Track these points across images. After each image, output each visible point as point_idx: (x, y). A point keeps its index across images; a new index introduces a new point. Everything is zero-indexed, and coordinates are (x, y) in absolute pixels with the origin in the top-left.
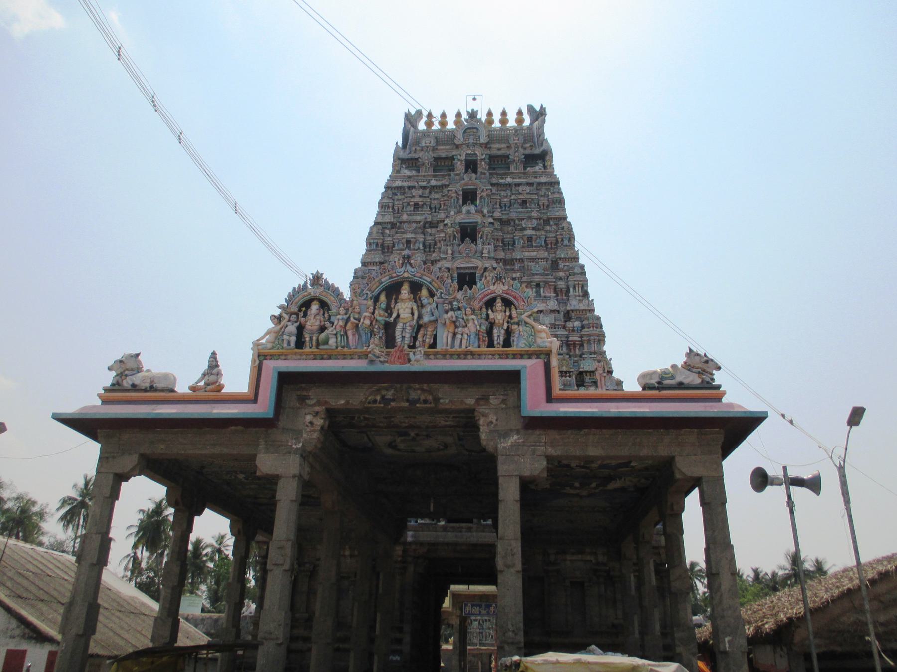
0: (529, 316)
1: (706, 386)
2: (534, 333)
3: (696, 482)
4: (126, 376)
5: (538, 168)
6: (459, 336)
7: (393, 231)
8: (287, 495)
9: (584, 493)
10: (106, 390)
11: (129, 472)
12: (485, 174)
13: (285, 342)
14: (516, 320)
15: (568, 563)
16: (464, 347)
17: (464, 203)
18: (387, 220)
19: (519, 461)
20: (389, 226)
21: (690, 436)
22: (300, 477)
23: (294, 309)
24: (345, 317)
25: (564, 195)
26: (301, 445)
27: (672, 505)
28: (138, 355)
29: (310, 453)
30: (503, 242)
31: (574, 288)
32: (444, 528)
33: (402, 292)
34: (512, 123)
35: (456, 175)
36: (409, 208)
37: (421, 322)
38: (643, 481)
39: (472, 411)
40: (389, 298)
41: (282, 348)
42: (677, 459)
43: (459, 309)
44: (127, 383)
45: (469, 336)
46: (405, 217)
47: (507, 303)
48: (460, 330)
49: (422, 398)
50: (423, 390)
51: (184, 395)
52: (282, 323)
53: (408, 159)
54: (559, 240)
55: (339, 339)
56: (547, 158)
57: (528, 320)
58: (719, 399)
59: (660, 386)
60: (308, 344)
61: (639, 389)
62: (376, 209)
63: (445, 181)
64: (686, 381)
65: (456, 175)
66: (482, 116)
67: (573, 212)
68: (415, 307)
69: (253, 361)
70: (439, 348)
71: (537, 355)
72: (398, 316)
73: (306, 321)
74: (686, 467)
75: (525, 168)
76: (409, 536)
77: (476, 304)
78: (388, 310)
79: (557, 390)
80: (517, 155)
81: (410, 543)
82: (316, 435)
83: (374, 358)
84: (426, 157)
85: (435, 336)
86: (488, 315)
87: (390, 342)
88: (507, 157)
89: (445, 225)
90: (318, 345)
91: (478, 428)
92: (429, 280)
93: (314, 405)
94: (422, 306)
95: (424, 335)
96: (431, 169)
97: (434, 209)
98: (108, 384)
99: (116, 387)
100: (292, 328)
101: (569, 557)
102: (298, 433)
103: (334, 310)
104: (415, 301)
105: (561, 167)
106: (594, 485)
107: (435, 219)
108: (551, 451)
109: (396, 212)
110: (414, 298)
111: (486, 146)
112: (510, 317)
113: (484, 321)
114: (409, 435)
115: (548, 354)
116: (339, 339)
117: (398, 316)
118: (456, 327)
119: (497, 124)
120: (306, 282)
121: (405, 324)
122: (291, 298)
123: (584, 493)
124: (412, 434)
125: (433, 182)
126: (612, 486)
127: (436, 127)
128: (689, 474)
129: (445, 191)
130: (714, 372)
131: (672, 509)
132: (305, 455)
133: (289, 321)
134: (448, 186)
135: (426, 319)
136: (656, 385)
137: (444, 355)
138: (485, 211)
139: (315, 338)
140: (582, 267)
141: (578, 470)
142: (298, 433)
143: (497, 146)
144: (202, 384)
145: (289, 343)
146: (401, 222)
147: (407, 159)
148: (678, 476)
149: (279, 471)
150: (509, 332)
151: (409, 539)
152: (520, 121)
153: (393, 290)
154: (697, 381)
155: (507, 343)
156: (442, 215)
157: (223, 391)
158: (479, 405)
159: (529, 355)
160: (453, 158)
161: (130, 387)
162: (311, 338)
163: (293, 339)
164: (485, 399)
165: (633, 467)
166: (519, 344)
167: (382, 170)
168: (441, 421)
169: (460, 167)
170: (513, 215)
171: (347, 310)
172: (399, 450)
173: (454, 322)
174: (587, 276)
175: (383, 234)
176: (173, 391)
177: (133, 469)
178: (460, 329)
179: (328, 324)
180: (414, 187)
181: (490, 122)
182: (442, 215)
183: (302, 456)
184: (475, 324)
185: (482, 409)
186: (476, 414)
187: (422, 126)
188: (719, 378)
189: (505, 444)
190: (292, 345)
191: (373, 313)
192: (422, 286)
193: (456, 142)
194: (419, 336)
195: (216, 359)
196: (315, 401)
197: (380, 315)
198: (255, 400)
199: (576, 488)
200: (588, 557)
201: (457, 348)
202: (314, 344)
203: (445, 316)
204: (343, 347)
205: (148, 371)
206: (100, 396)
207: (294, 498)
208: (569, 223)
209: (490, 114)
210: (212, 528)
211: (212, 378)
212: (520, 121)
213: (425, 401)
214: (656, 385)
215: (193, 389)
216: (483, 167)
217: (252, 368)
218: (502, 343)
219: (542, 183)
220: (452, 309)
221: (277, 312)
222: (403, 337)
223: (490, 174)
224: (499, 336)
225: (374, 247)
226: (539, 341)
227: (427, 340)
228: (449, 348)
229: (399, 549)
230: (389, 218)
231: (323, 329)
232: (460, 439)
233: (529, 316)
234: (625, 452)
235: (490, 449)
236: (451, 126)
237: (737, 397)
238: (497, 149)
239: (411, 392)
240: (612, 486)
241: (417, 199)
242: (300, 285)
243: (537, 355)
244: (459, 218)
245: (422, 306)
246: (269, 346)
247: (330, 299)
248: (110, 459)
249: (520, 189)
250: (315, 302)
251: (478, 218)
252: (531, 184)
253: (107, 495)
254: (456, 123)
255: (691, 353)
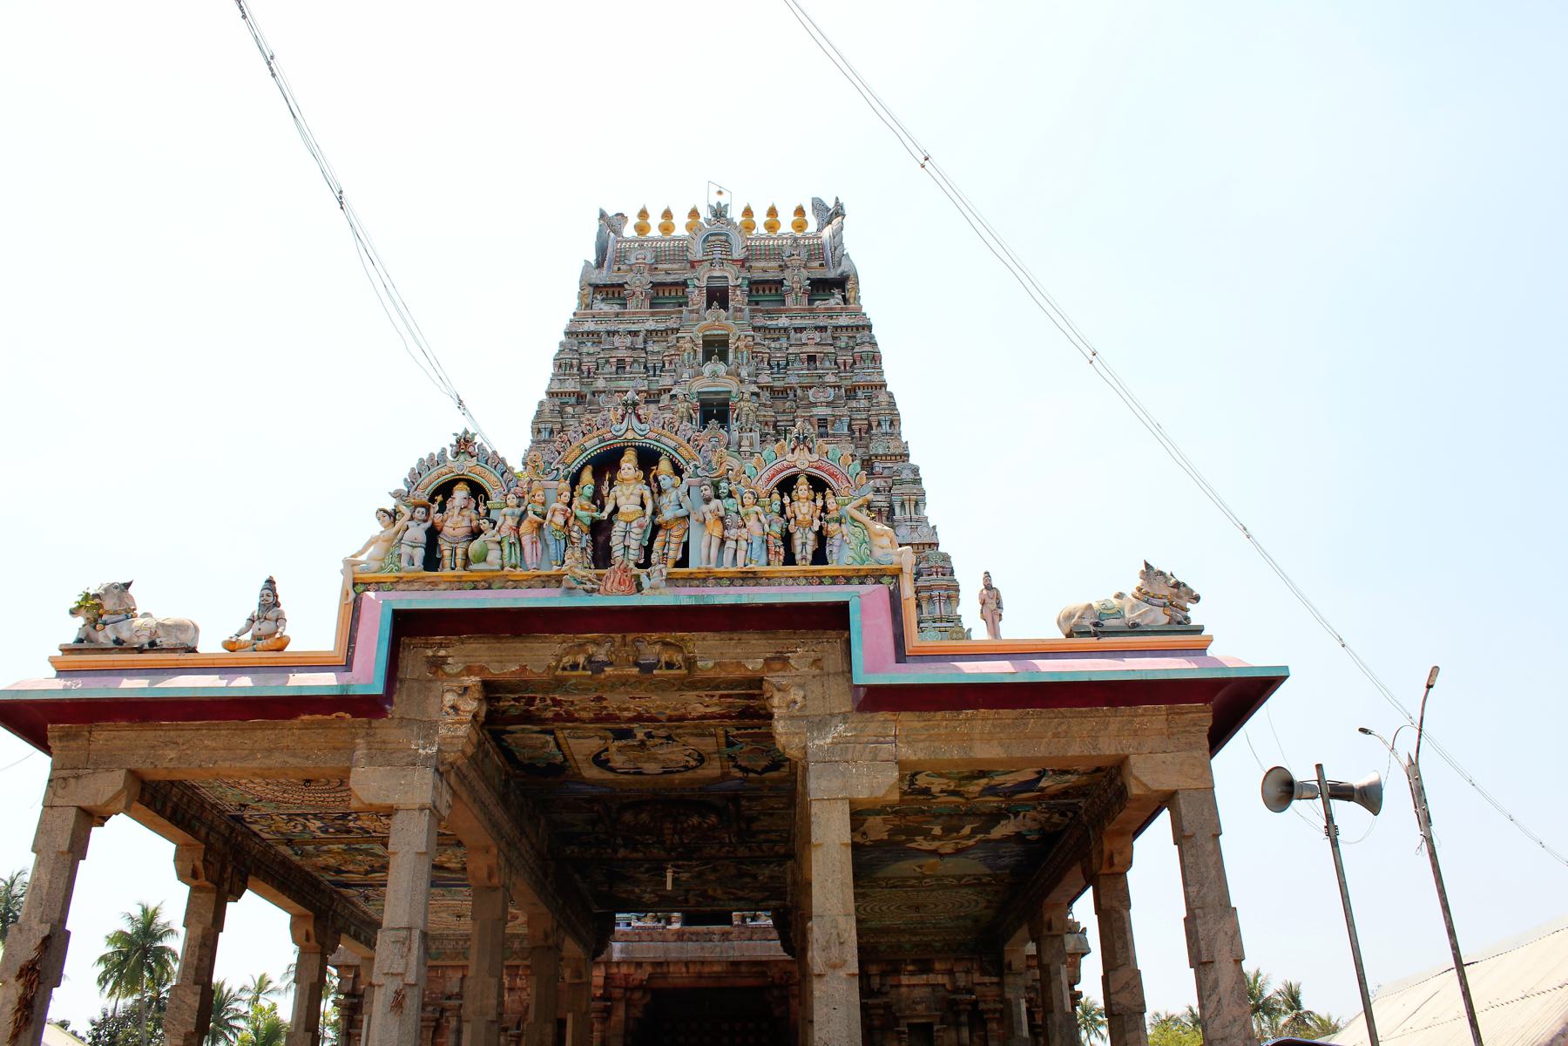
0: (859, 508)
1: (1178, 628)
2: (868, 540)
3: (1167, 800)
4: (105, 624)
5: (835, 301)
6: (730, 544)
7: (579, 409)
8: (409, 842)
9: (948, 847)
10: (67, 650)
11: (107, 804)
12: (741, 310)
13: (404, 560)
14: (834, 515)
15: (904, 990)
16: (740, 563)
17: (707, 358)
18: (571, 390)
19: (844, 773)
20: (573, 400)
21: (1154, 717)
22: (434, 810)
23: (424, 497)
24: (518, 511)
25: (881, 347)
26: (435, 749)
27: (1111, 856)
28: (127, 585)
29: (452, 764)
30: (775, 427)
31: (903, 505)
32: (680, 936)
33: (623, 465)
34: (786, 226)
35: (691, 312)
36: (608, 369)
37: (659, 520)
38: (1056, 818)
39: (757, 682)
40: (598, 476)
41: (399, 570)
42: (1132, 759)
43: (730, 495)
44: (105, 636)
45: (750, 544)
46: (600, 384)
47: (818, 485)
48: (732, 533)
49: (664, 658)
50: (665, 644)
51: (213, 657)
52: (398, 524)
53: (605, 286)
54: (874, 424)
55: (506, 551)
56: (849, 286)
57: (857, 514)
58: (1200, 650)
59: (1099, 630)
60: (447, 562)
61: (1059, 635)
62: (549, 369)
63: (672, 324)
64: (1143, 622)
65: (691, 312)
66: (736, 215)
67: (897, 374)
68: (647, 493)
69: (345, 594)
70: (695, 564)
71: (877, 576)
72: (616, 509)
73: (443, 521)
74: (1147, 774)
75: (811, 302)
76: (617, 950)
77: (762, 487)
78: (597, 499)
79: (914, 640)
80: (797, 279)
81: (618, 964)
82: (463, 730)
83: (574, 584)
84: (639, 283)
85: (686, 546)
86: (783, 506)
87: (602, 556)
88: (781, 282)
89: (673, 397)
90: (467, 561)
91: (770, 716)
92: (673, 444)
93: (459, 674)
94: (660, 492)
95: (665, 543)
96: (647, 303)
97: (651, 370)
98: (70, 638)
99: (85, 645)
100: (418, 533)
101: (905, 980)
102: (428, 728)
103: (495, 499)
104: (648, 484)
105: (872, 299)
106: (967, 830)
107: (654, 387)
108: (906, 752)
109: (588, 375)
110: (646, 477)
111: (743, 263)
112: (824, 509)
113: (775, 517)
114: (635, 736)
115: (896, 575)
116: (506, 551)
117: (616, 509)
118: (725, 527)
119: (760, 229)
120: (444, 450)
121: (629, 523)
122: (415, 477)
123: (948, 847)
124: (640, 735)
125: (651, 325)
126: (998, 832)
127: (655, 232)
128: (1155, 786)
129: (672, 338)
130: (1189, 605)
131: (1111, 864)
132: (443, 770)
133: (412, 519)
134: (678, 330)
135: (668, 514)
136: (1092, 628)
137: (704, 578)
138: (744, 373)
139: (460, 552)
140: (916, 470)
141: (944, 798)
142: (428, 728)
143: (763, 264)
144: (247, 637)
145: (411, 561)
146: (593, 394)
147: (602, 290)
148: (1135, 790)
149: (394, 799)
150: (821, 537)
151: (616, 956)
152: (800, 225)
153: (606, 464)
154: (1160, 618)
155: (820, 557)
156: (666, 381)
157: (287, 649)
158: (770, 670)
159: (862, 578)
160: (685, 284)
161: (112, 645)
162: (454, 551)
163: (420, 553)
164: (782, 660)
165: (1042, 789)
166: (842, 557)
167: (557, 305)
168: (696, 704)
169: (697, 298)
170: (793, 380)
171: (521, 498)
172: (612, 770)
173: (722, 519)
174: (925, 485)
175: (561, 412)
176: (194, 650)
177: (115, 798)
178: (733, 531)
179: (485, 524)
180: (614, 333)
181: (749, 226)
182: (666, 381)
183: (437, 770)
184: (759, 524)
185: (773, 678)
186: (766, 686)
187: (629, 232)
188: (1196, 615)
189: (821, 742)
190: (419, 561)
191: (570, 504)
192: (660, 454)
193: (690, 257)
194: (657, 545)
195: (274, 590)
196: (461, 667)
197: (583, 509)
198: (348, 666)
199: (935, 838)
200: (941, 979)
201: (727, 567)
202: (459, 561)
203: (705, 508)
204: (515, 567)
205: (146, 615)
206: (53, 661)
207: (423, 849)
208: (891, 395)
209: (748, 212)
210: (258, 943)
211: (266, 627)
212: (800, 225)
213: (670, 665)
214: (1092, 628)
215: (231, 646)
216: (737, 299)
217: (343, 606)
218: (810, 557)
219: (841, 327)
220: (718, 497)
221: (390, 505)
222: (626, 548)
223: (752, 311)
224: (804, 544)
225: (545, 435)
226: (878, 553)
227: (671, 554)
228: (712, 565)
229: (598, 975)
230: (571, 385)
231: (475, 533)
232: (730, 744)
233: (859, 508)
234: (1042, 749)
235: (793, 753)
236: (680, 230)
237: (1233, 648)
238: (765, 269)
239: (642, 646)
240: (998, 832)
241: (621, 354)
242: (432, 455)
243: (877, 576)
244: (700, 385)
245: (660, 492)
246: (375, 565)
247: (489, 480)
248: (72, 781)
249: (804, 336)
250: (461, 485)
251: (732, 385)
252: (823, 329)
253: (65, 847)
254: (689, 227)
255: (1149, 571)
